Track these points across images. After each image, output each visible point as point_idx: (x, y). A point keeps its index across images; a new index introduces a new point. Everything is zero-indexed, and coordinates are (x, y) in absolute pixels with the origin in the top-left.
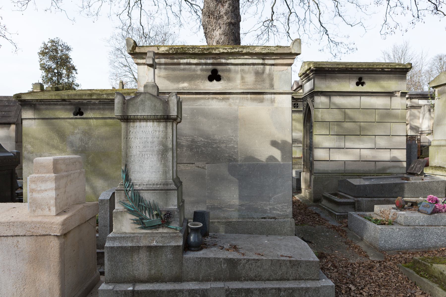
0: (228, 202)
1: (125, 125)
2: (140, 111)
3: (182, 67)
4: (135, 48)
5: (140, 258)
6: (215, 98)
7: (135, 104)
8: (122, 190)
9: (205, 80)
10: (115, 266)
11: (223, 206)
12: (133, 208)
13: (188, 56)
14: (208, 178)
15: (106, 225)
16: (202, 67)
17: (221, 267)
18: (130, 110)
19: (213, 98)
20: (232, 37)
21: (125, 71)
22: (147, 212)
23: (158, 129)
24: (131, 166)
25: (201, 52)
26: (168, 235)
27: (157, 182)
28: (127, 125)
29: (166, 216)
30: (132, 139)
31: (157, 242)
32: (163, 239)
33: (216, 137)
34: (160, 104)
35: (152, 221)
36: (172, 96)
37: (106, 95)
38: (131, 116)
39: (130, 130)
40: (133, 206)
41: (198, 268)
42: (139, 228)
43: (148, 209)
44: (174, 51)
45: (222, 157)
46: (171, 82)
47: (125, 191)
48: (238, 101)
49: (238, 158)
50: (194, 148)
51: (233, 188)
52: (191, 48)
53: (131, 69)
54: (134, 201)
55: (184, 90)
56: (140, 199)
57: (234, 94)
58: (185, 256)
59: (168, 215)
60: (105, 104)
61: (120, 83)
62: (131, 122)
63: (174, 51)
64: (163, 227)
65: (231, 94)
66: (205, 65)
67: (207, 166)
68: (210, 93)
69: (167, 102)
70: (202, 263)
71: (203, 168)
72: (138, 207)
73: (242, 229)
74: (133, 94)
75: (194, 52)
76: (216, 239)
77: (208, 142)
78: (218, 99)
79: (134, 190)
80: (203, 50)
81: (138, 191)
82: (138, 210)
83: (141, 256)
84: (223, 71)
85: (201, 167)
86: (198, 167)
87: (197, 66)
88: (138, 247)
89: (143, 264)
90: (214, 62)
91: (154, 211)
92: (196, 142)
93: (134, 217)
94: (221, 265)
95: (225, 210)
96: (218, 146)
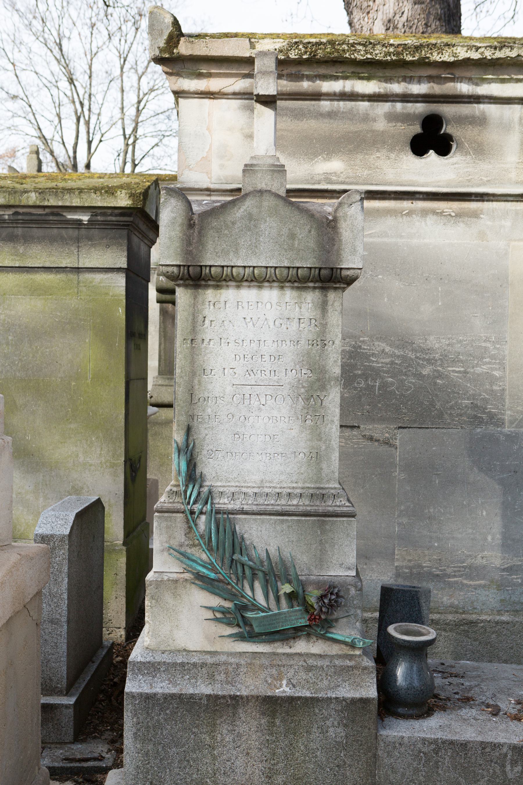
0: (468, 556)
1: (188, 295)
2: (243, 252)
3: (325, 105)
4: (175, 40)
5: (239, 735)
6: (434, 212)
7: (227, 227)
8: (178, 512)
9: (401, 150)
10: (156, 758)
11: (449, 571)
12: (213, 569)
13: (351, 69)
14: (403, 476)
15: (58, 617)
16: (394, 106)
17: (504, 772)
18: (210, 246)
19: (425, 213)
20: (438, 6)
21: (10, 114)
22: (257, 585)
23: (296, 313)
24: (206, 432)
25: (394, 58)
26: (326, 663)
27: (289, 488)
28: (195, 298)
29: (326, 601)
30: (212, 343)
31: (294, 686)
32: (310, 674)
33: (433, 342)
34: (310, 231)
35: (275, 615)
36: (350, 202)
37: (36, 192)
38: (211, 266)
39: (206, 312)
40: (213, 563)
41: (426, 773)
42: (230, 636)
43: (260, 574)
44: (306, 52)
45: (452, 408)
46: (289, 154)
47: (188, 513)
48: (508, 223)
49: (503, 414)
50: (360, 376)
51: (484, 513)
52: (359, 44)
53: (30, 106)
54: (218, 548)
55: (331, 182)
56: (236, 540)
57: (497, 201)
58: (384, 733)
59: (333, 597)
60: (32, 221)
61: (31, 152)
62: (207, 287)
63: (306, 52)
64: (309, 635)
65: (488, 201)
66: (402, 101)
67: (399, 436)
68: (417, 196)
69: (333, 223)
70: (441, 757)
71: (387, 443)
72: (231, 567)
73: (512, 648)
74: (123, 191)
75: (369, 56)
76: (462, 681)
77: (404, 358)
78: (441, 214)
79: (218, 512)
80: (400, 49)
81: (230, 516)
82: (231, 578)
83: (242, 728)
84: (462, 120)
85: (378, 441)
86: (371, 439)
87: (376, 104)
88: (234, 698)
89: (248, 754)
90: (431, 92)
91: (283, 584)
92: (367, 357)
93: (215, 601)
94: (503, 766)
95: (456, 583)
96: (438, 371)
